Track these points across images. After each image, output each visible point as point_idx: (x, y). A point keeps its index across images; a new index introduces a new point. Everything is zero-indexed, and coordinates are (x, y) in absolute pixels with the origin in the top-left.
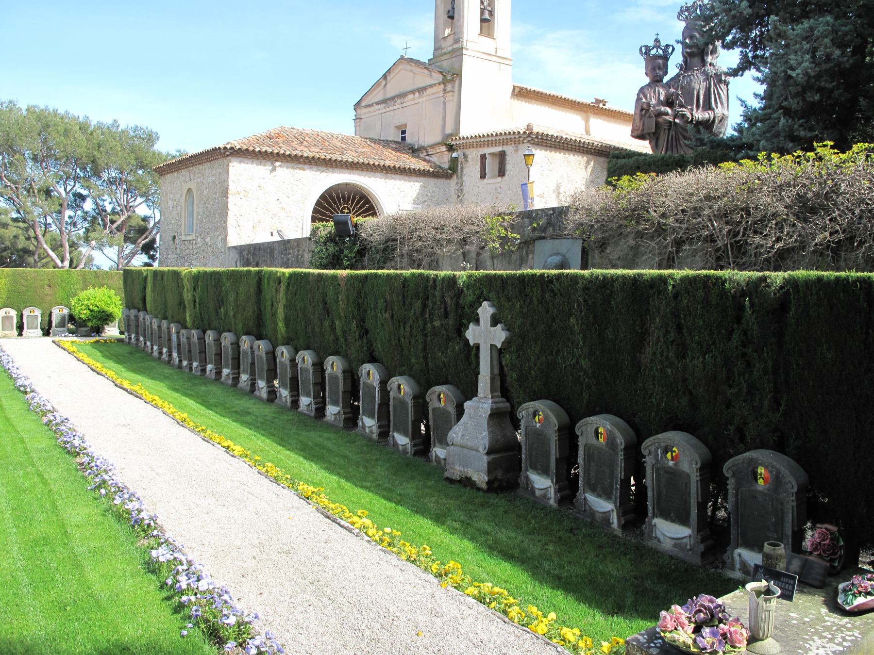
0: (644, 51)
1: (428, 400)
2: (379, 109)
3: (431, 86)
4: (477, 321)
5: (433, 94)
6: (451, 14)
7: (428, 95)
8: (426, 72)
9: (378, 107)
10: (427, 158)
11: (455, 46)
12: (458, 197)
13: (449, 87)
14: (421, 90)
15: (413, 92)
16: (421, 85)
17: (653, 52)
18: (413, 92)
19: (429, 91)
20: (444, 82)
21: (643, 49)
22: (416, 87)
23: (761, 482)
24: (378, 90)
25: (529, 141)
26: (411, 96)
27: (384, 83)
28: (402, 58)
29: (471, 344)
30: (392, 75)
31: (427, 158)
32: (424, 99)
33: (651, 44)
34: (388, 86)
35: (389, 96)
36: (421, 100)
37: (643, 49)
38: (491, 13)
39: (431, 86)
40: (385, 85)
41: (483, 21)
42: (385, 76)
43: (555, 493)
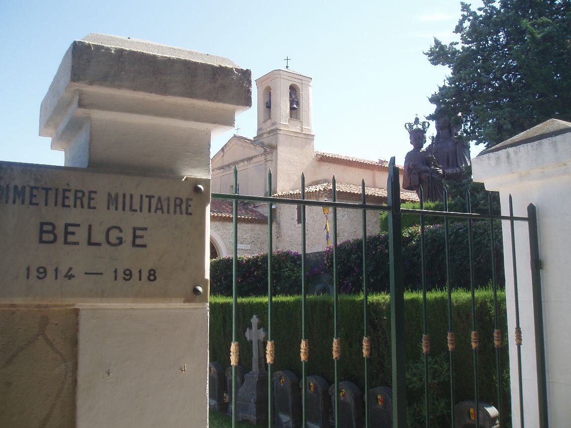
0: (408, 127)
1: (226, 375)
2: (219, 173)
3: (255, 157)
4: (251, 327)
5: (257, 162)
6: (268, 105)
7: (254, 163)
8: (252, 146)
9: (218, 171)
10: (254, 209)
11: (273, 128)
12: (278, 237)
13: (269, 157)
14: (249, 159)
15: (243, 161)
16: (249, 156)
17: (415, 127)
18: (243, 161)
19: (254, 160)
20: (265, 153)
21: (407, 125)
22: (245, 157)
23: (380, 403)
24: (219, 158)
25: (326, 196)
26: (241, 164)
27: (222, 154)
28: (235, 136)
29: (248, 339)
30: (228, 148)
31: (254, 209)
32: (252, 165)
33: (412, 121)
34: (225, 156)
35: (226, 163)
36: (249, 167)
37: (407, 125)
38: (298, 104)
39: (255, 157)
40: (223, 155)
41: (292, 109)
42: (223, 150)
43: (292, 424)
